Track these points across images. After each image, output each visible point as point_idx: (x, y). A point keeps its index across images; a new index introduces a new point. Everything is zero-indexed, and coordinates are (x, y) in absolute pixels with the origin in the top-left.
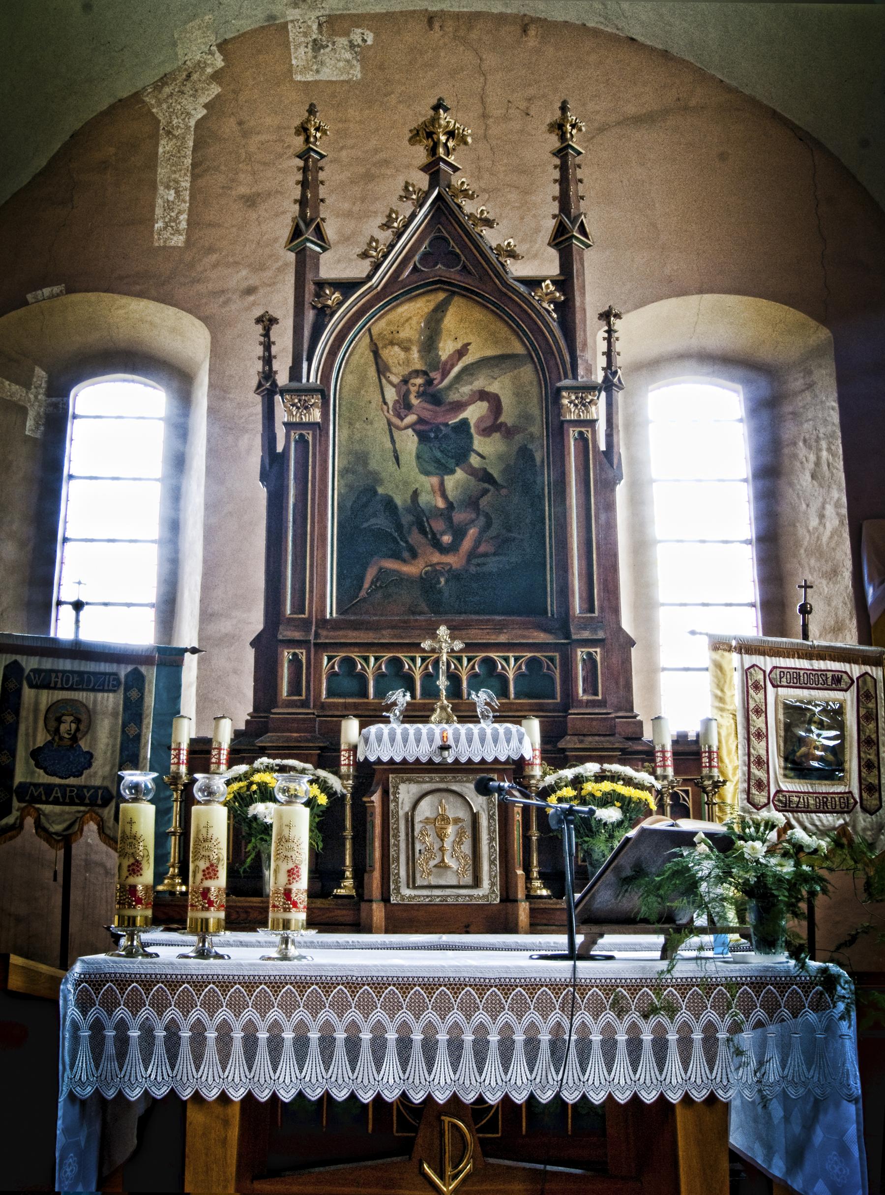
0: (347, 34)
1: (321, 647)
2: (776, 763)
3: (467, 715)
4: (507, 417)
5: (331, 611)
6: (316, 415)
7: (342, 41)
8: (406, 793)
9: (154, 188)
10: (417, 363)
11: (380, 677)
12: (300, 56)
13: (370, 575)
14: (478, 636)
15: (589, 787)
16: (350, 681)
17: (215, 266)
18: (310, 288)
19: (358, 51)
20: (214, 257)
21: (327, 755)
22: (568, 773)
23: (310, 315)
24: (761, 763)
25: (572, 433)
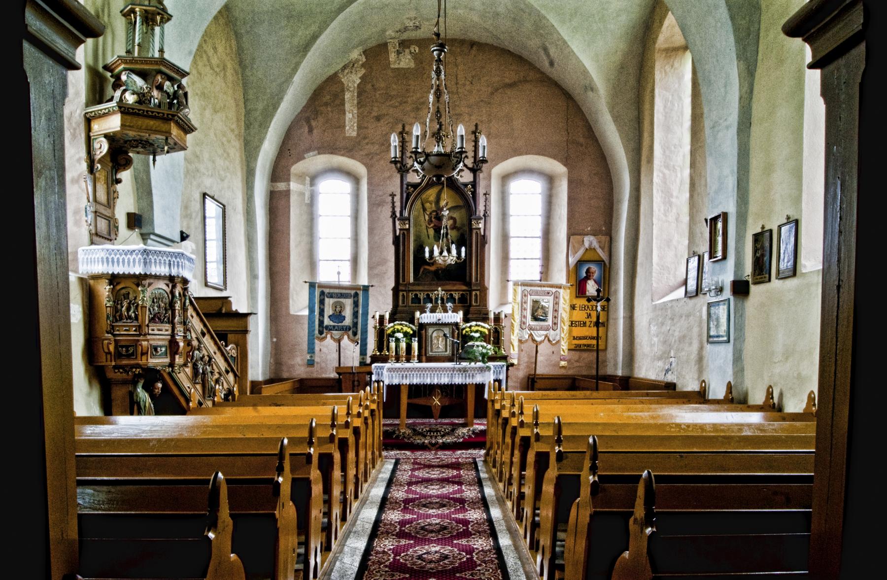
0: (409, 47)
1: (410, 291)
2: (529, 316)
3: (446, 311)
4: (458, 225)
5: (412, 280)
6: (407, 226)
7: (407, 51)
8: (430, 330)
9: (344, 114)
10: (434, 209)
11: (424, 299)
12: (392, 57)
13: (422, 270)
14: (448, 287)
15: (473, 328)
16: (416, 300)
17: (367, 144)
18: (405, 186)
19: (415, 57)
20: (366, 141)
21: (412, 321)
22: (468, 325)
23: (405, 195)
24: (525, 317)
25: (474, 231)
